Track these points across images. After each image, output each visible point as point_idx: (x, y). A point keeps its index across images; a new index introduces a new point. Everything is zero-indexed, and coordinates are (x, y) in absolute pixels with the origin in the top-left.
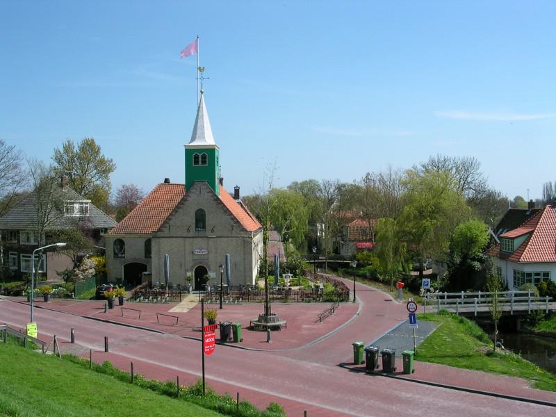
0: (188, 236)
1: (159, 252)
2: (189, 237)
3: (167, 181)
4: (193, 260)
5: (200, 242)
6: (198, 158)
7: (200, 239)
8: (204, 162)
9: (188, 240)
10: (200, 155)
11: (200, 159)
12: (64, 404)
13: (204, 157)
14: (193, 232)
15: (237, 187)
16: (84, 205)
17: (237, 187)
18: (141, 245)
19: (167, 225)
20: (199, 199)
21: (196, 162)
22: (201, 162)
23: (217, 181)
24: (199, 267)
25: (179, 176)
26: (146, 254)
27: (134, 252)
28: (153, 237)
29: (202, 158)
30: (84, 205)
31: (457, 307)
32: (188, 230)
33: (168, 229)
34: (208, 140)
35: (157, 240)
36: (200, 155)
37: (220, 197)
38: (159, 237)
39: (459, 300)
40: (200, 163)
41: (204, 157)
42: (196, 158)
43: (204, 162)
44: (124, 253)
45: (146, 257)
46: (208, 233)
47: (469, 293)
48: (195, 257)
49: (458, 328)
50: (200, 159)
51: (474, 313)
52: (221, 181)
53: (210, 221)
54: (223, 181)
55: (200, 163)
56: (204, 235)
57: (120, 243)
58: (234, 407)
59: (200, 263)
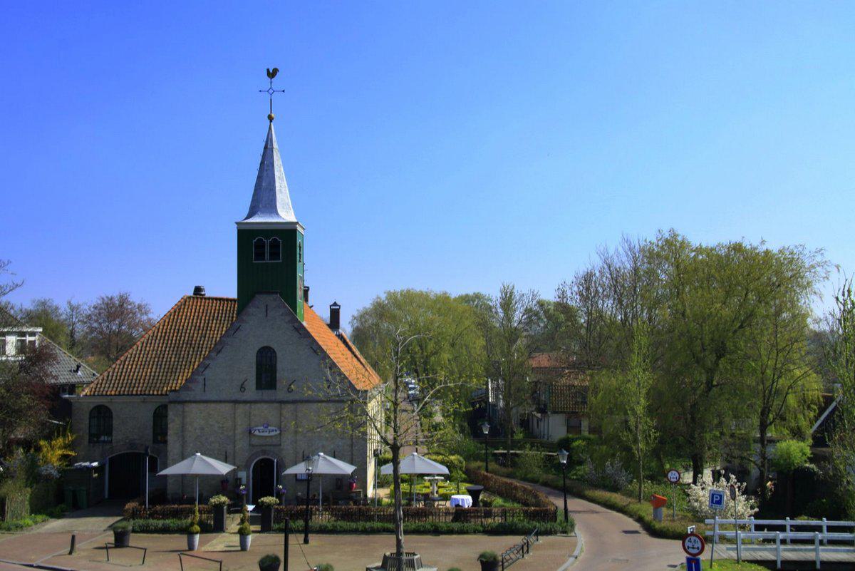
0: (244, 398)
1: (183, 431)
2: (245, 402)
3: (198, 290)
4: (251, 445)
5: (265, 412)
6: (271, 254)
7: (265, 406)
8: (274, 255)
9: (241, 409)
10: (267, 242)
11: (267, 249)
12: (826, 320)
13: (275, 245)
14: (251, 392)
15: (335, 304)
16: (28, 339)
17: (335, 304)
18: (145, 415)
19: (200, 378)
20: (261, 330)
21: (260, 255)
22: (269, 257)
23: (300, 293)
24: (262, 459)
25: (223, 282)
26: (155, 435)
27: (131, 427)
28: (171, 402)
29: (271, 246)
30: (28, 339)
31: (776, 549)
32: (242, 388)
33: (201, 386)
34: (286, 213)
35: (179, 407)
36: (267, 242)
37: (305, 324)
38: (183, 402)
39: (781, 535)
40: (267, 255)
41: (275, 245)
42: (260, 246)
43: (274, 255)
44: (110, 434)
45: (155, 441)
46: (281, 394)
47: (798, 522)
48: (255, 441)
49: (657, 303)
50: (267, 249)
51: (814, 563)
52: (306, 291)
53: (285, 368)
54: (310, 293)
55: (267, 255)
56: (273, 398)
57: (102, 415)
58: (539, 537)
59: (264, 452)
